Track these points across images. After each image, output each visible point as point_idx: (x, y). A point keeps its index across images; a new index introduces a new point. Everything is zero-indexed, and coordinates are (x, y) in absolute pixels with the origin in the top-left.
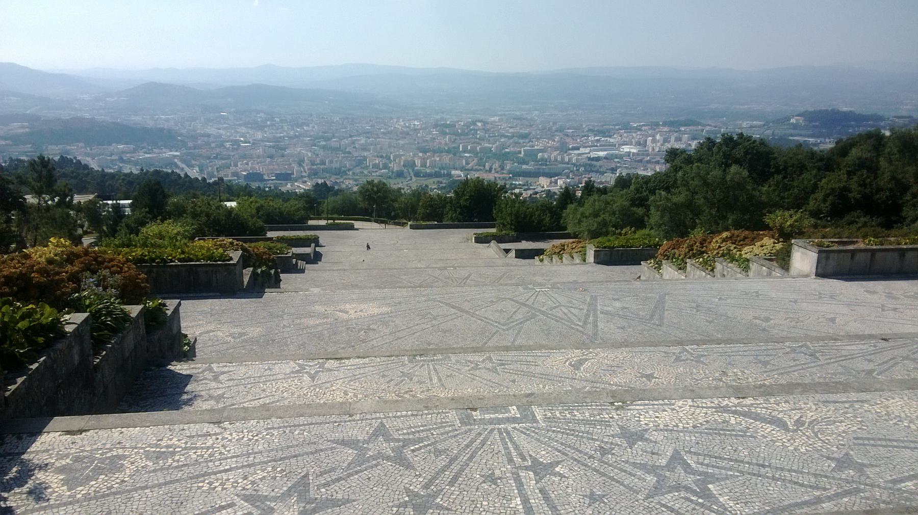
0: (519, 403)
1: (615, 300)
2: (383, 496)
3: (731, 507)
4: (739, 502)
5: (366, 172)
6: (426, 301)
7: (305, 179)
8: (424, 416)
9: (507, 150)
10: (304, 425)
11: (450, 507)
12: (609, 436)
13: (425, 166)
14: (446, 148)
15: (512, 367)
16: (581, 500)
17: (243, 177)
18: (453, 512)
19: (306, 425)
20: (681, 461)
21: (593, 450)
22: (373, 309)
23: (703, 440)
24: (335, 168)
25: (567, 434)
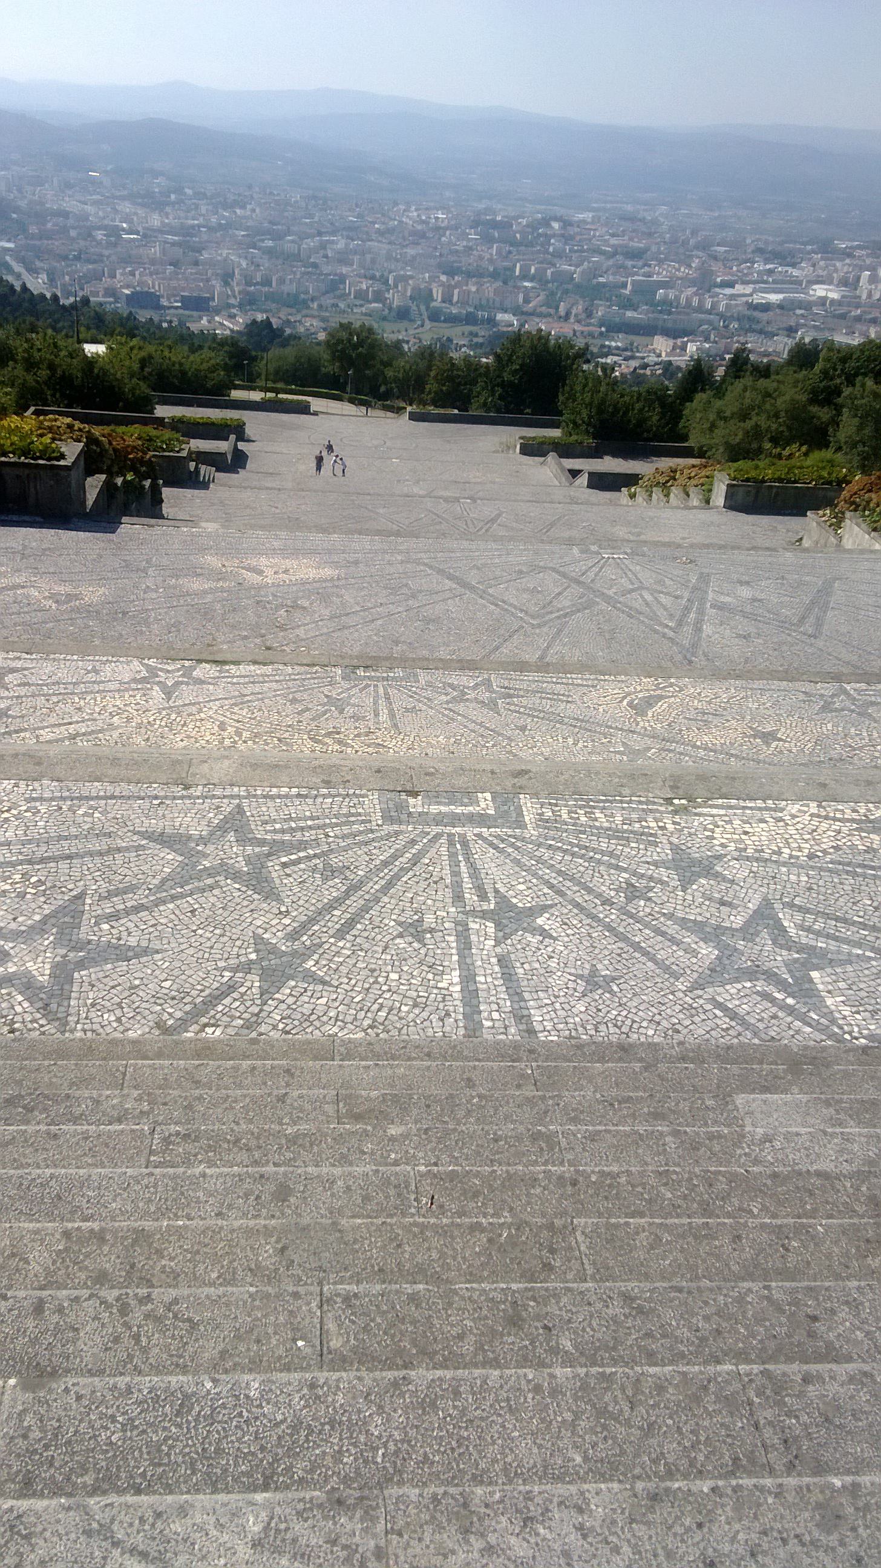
0: (498, 788)
1: (741, 583)
2: (212, 948)
3: (845, 1018)
4: (861, 1009)
5: (342, 305)
6: (402, 562)
7: (234, 311)
8: (320, 800)
9: (601, 280)
10: (98, 798)
11: (327, 978)
12: (648, 863)
13: (451, 302)
14: (491, 269)
15: (524, 701)
16: (571, 985)
17: (124, 298)
18: (331, 989)
19: (102, 798)
20: (771, 922)
21: (614, 889)
22: (306, 570)
23: (821, 883)
24: (288, 294)
25: (573, 855)
